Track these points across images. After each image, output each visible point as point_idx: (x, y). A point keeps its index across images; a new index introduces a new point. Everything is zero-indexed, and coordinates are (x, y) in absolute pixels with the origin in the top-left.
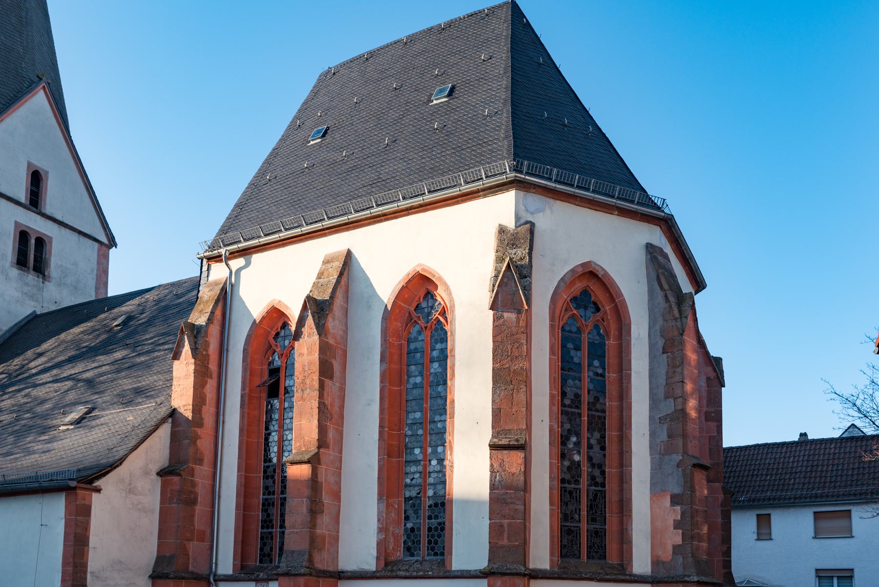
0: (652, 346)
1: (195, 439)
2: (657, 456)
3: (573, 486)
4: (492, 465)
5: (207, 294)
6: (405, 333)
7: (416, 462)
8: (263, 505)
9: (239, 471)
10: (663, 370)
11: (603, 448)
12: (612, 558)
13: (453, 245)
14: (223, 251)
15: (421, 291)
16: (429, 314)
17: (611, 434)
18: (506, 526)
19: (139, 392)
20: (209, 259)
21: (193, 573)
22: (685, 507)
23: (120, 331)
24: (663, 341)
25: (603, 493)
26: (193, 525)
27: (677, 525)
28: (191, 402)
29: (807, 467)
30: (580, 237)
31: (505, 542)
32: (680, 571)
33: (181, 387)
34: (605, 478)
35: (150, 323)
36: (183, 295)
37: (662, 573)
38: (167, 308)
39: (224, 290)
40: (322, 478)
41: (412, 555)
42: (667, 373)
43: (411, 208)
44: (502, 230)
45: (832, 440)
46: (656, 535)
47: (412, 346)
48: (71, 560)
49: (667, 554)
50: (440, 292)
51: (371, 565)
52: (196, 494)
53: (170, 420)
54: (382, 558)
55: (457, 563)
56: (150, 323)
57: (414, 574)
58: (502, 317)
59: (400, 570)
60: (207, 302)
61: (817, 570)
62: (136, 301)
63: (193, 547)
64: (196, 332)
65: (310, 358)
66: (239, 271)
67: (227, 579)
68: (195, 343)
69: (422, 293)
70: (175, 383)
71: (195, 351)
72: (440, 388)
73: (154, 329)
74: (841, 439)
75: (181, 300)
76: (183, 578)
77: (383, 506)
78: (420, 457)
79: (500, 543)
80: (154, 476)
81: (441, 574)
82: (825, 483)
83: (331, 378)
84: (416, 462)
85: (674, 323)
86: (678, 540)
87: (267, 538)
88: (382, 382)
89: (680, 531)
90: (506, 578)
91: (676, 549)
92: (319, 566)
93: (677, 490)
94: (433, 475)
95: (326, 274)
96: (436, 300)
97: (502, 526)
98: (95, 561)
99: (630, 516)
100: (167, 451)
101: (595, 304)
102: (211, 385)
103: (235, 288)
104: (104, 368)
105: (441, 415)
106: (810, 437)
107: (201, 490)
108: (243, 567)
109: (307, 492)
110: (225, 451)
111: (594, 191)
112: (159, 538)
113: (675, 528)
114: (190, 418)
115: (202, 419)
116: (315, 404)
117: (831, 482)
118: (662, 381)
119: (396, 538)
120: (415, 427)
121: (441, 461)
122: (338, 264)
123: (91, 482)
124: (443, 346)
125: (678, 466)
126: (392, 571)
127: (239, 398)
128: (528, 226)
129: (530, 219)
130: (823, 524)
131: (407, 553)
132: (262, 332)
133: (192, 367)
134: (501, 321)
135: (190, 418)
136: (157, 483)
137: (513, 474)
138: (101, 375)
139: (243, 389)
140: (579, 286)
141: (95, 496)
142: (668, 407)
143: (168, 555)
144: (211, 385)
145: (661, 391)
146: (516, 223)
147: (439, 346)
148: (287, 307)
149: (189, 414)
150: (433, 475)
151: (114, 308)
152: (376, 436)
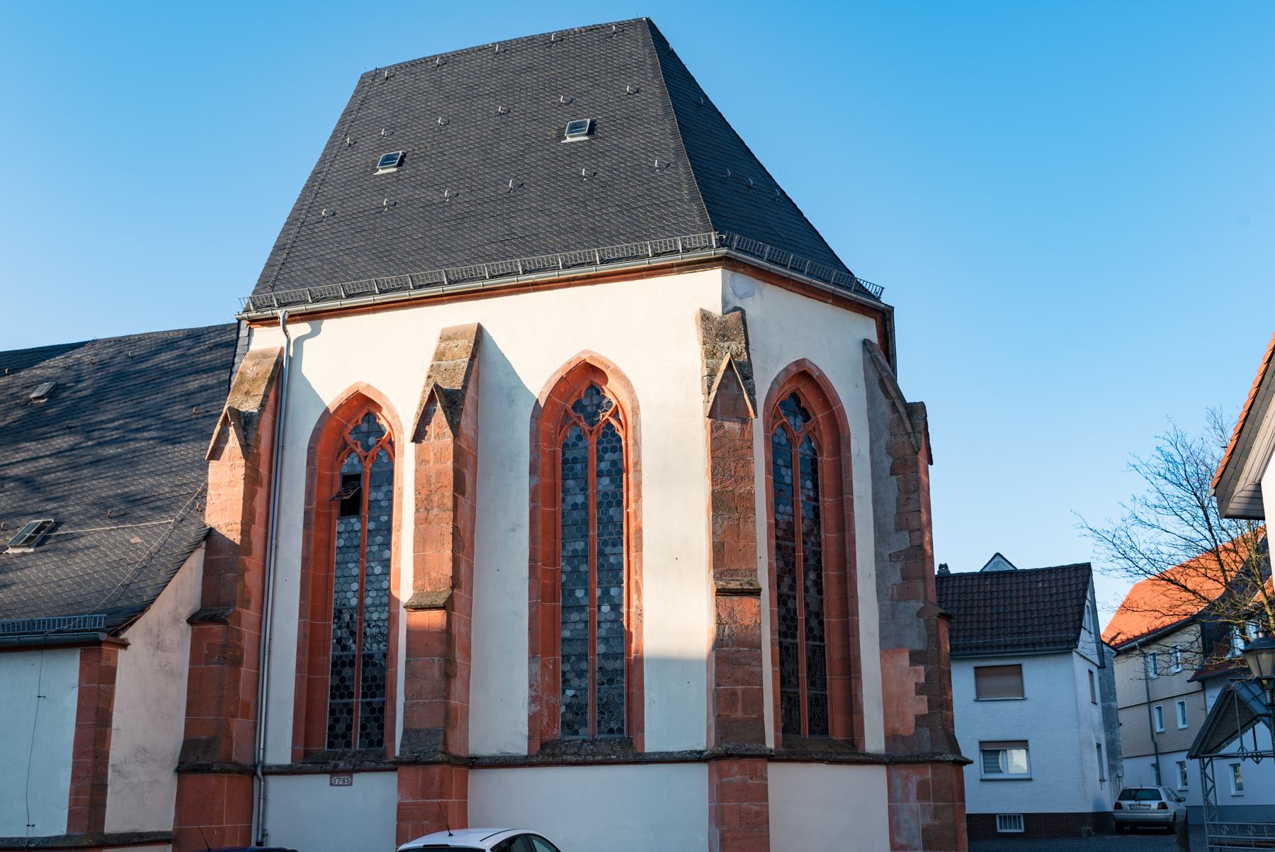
0: (875, 466)
1: (241, 572)
2: (888, 603)
3: (789, 640)
4: (718, 615)
5: (251, 365)
6: (560, 438)
7: (581, 608)
8: (335, 664)
9: (301, 616)
10: (891, 496)
11: (820, 592)
12: (838, 734)
13: (651, 335)
14: (280, 313)
15: (584, 387)
16: (596, 414)
17: (830, 573)
18: (739, 693)
19: (132, 501)
20: (253, 321)
21: (236, 763)
22: (930, 667)
23: (47, 406)
24: (891, 460)
25: (822, 648)
26: (238, 695)
27: (920, 690)
28: (239, 519)
29: (959, 608)
30: (797, 331)
31: (739, 714)
32: (927, 748)
33: (223, 498)
34: (823, 631)
35: (100, 395)
36: (142, 359)
37: (901, 751)
38: (121, 376)
39: (278, 364)
40: (455, 630)
41: (576, 733)
42: (898, 500)
43: (574, 279)
44: (705, 317)
45: (973, 575)
46: (890, 702)
47: (569, 455)
48: (91, 748)
49: (907, 726)
50: (613, 389)
51: (519, 745)
52: (242, 650)
53: (204, 544)
54: (537, 738)
55: (652, 743)
56: (100, 395)
57: (590, 758)
58: (722, 426)
59: (565, 753)
60: (254, 380)
61: (981, 743)
62: (58, 361)
63: (238, 726)
64: (245, 423)
65: (439, 466)
66: (300, 340)
67: (772, 758)
68: (246, 438)
69: (584, 387)
70: (211, 491)
71: (247, 449)
72: (611, 511)
73: (109, 407)
74: (983, 575)
75: (144, 366)
76: (229, 771)
77: (537, 668)
78: (585, 602)
79: (734, 716)
80: (184, 625)
81: (631, 758)
82: (985, 629)
83: (463, 494)
84: (581, 608)
85: (905, 438)
86: (923, 708)
87: (341, 712)
88: (532, 500)
89: (925, 697)
90: (745, 761)
91: (920, 720)
92: (454, 750)
93: (919, 646)
94: (603, 625)
95: (448, 354)
96: (604, 397)
97: (734, 693)
98: (118, 750)
99: (859, 679)
100: (199, 588)
101: (804, 410)
102: (261, 493)
103: (295, 364)
104: (42, 462)
105: (614, 545)
106: (953, 571)
107: (247, 645)
108: (307, 754)
109: (439, 648)
110: (278, 588)
111: (809, 274)
112: (188, 713)
113: (1018, 692)
114: (238, 541)
115: (250, 543)
116: (448, 529)
117: (992, 629)
118: (891, 509)
119: (553, 710)
120: (576, 561)
121: (616, 607)
122: (467, 343)
123: (116, 634)
124: (615, 456)
125: (919, 615)
126: (553, 755)
127: (302, 514)
128: (738, 313)
129: (739, 305)
130: (988, 682)
131: (566, 730)
132: (334, 424)
133: (243, 471)
134: (721, 432)
135: (238, 541)
136: (186, 631)
137: (747, 627)
138: (47, 471)
139: (308, 501)
140: (789, 388)
141: (121, 653)
142: (901, 542)
143: (204, 737)
144: (261, 493)
145: (891, 521)
146: (724, 307)
147: (608, 456)
148: (381, 394)
149: (236, 537)
150: (606, 626)
151: (19, 369)
152: (526, 573)
